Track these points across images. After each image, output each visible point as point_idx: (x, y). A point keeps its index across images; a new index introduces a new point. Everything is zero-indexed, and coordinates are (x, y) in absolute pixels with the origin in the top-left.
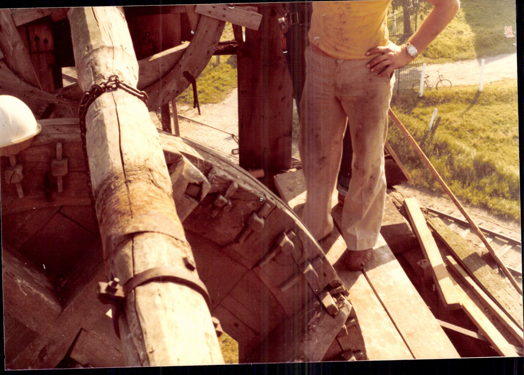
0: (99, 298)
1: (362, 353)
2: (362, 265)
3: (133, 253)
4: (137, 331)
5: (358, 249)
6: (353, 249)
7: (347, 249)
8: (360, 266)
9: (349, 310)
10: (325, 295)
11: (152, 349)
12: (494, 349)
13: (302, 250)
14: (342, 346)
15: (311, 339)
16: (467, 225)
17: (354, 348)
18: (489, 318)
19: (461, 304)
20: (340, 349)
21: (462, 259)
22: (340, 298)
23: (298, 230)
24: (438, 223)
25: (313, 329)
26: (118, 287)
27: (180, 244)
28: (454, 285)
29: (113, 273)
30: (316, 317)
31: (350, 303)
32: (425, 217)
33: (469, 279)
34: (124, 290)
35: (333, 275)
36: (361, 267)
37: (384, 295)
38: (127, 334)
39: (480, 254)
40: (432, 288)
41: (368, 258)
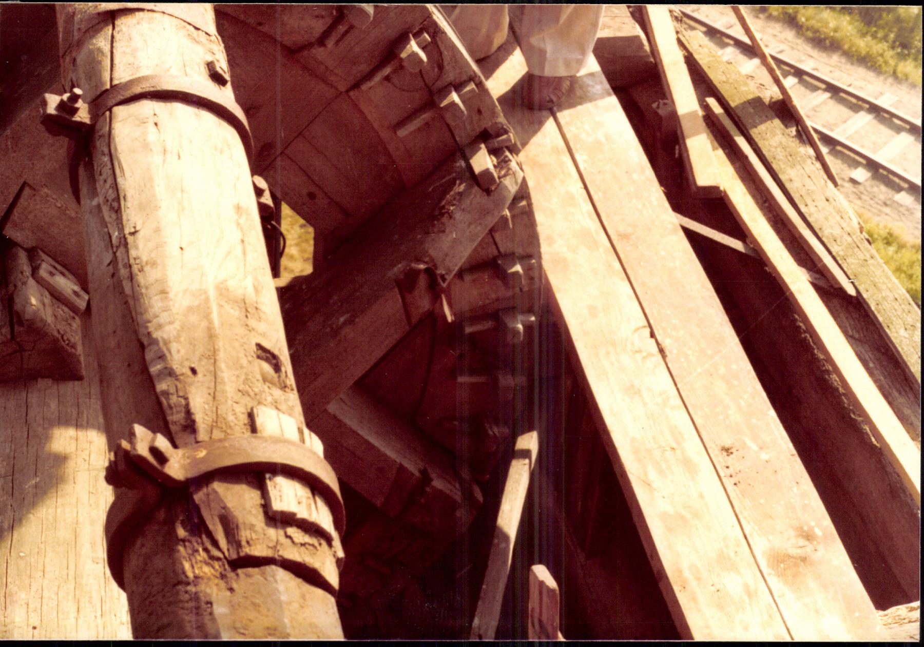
0: (43, 123)
1: (534, 261)
2: (551, 101)
3: (112, 47)
4: (110, 191)
5: (548, 72)
6: (537, 72)
7: (528, 73)
8: (548, 102)
9: (516, 182)
10: (476, 150)
11: (135, 227)
12: (770, 273)
13: (441, 67)
14: (500, 245)
15: (444, 231)
16: (751, 50)
17: (519, 251)
18: (769, 220)
19: (722, 188)
20: (496, 252)
21: (733, 104)
22: (503, 157)
23: (436, 31)
24: (699, 42)
25: (449, 214)
26: (80, 104)
27: (202, 37)
28: (714, 149)
29: (74, 79)
30: (457, 190)
31: (521, 169)
32: (675, 28)
33: (741, 141)
34: (91, 111)
35: (494, 113)
36: (550, 105)
37: (585, 157)
38: (92, 199)
39: (767, 101)
40: (675, 154)
41: (564, 90)
